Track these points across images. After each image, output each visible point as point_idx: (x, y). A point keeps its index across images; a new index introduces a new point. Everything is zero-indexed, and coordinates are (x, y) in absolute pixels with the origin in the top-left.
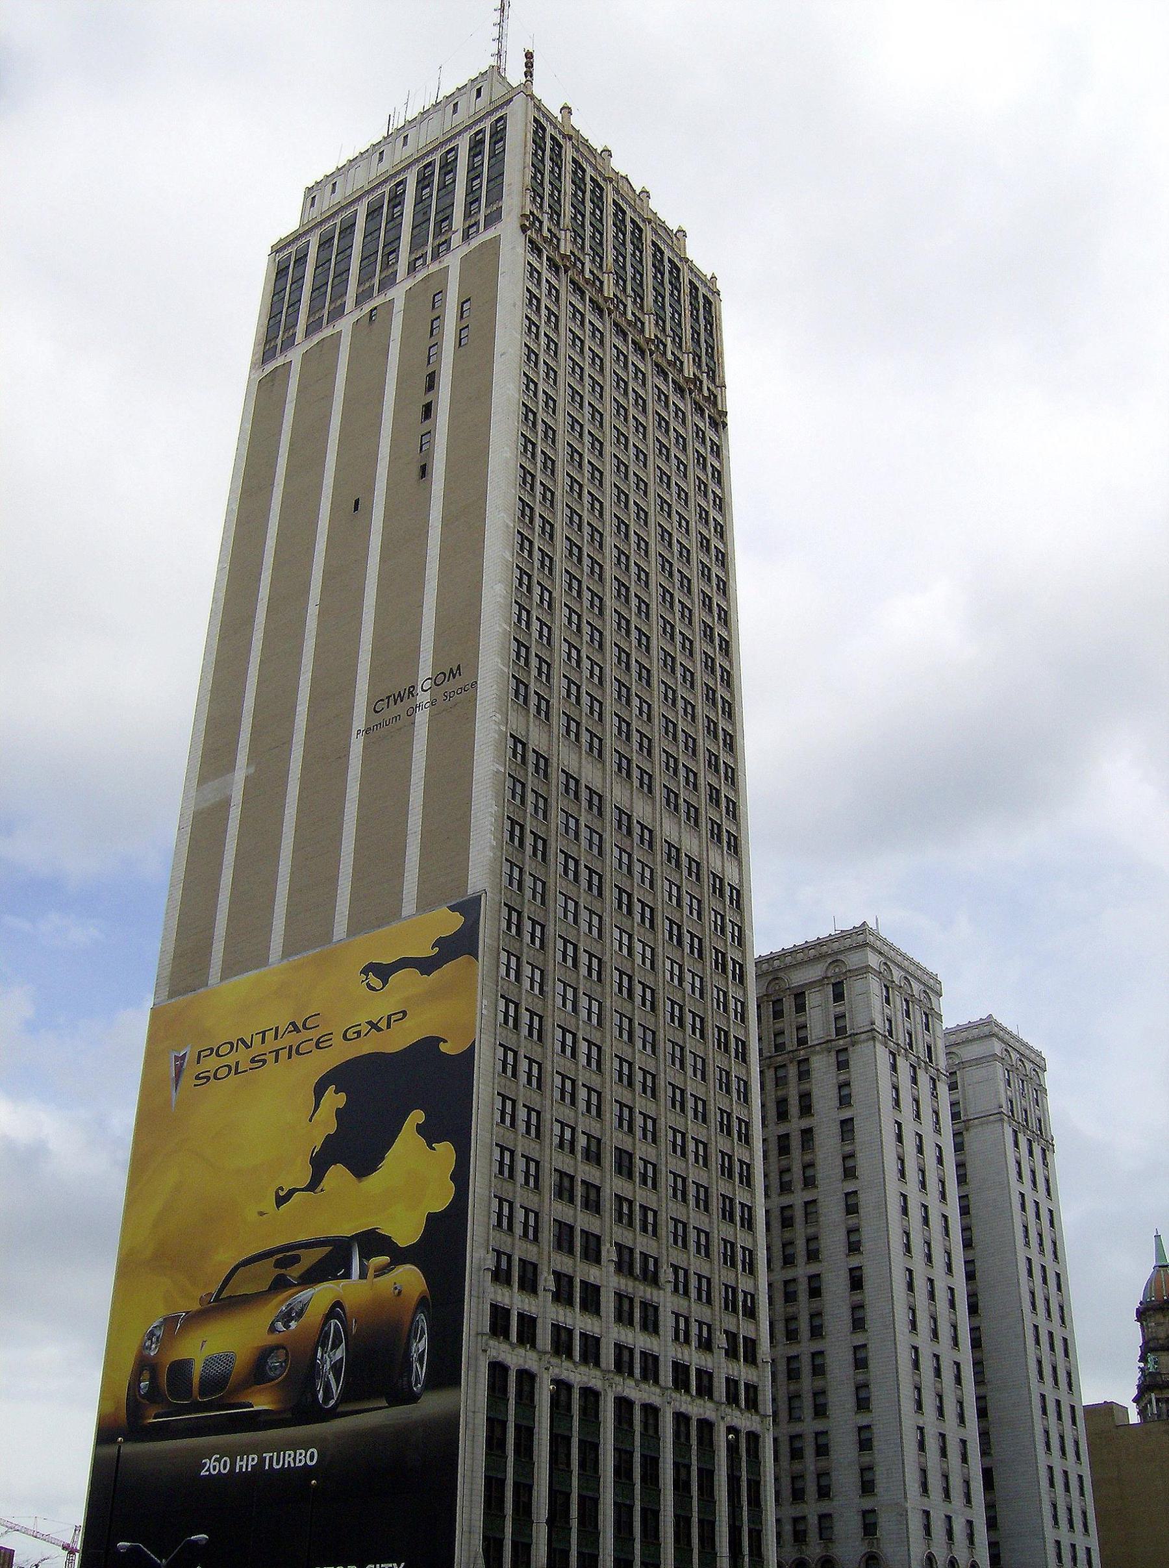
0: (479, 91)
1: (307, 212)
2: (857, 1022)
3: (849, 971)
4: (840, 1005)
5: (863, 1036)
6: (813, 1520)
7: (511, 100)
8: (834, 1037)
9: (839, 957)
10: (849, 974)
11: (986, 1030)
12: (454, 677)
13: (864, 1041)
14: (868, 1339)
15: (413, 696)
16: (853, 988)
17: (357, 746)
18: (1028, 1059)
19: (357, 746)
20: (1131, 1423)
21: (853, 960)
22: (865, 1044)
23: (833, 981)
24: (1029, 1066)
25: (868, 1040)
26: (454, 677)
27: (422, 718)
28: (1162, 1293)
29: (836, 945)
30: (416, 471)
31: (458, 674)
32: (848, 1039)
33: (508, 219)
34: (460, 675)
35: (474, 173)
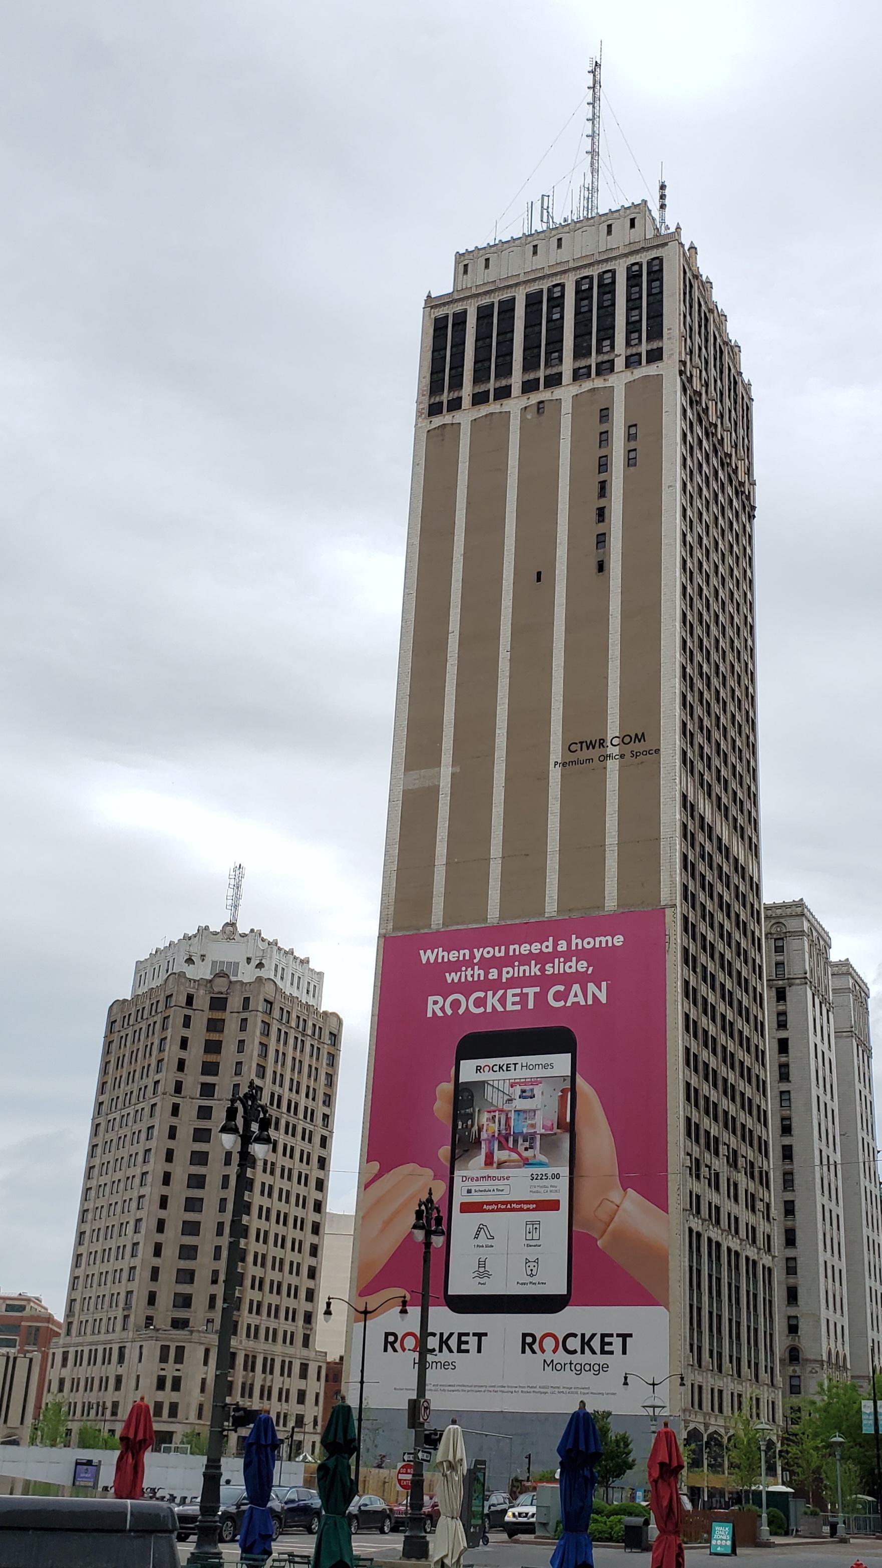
0: (632, 222)
1: (460, 279)
2: (793, 970)
3: (789, 932)
4: (780, 955)
5: (798, 981)
6: (109, 1405)
7: (666, 244)
8: (774, 977)
9: (782, 920)
10: (788, 934)
11: (844, 969)
12: (639, 741)
13: (798, 985)
14: (795, 1197)
15: (604, 747)
16: (791, 944)
17: (555, 775)
18: (864, 992)
19: (555, 775)
20: (430, 1308)
21: (792, 925)
22: (800, 987)
23: (775, 936)
24: (863, 994)
25: (801, 984)
26: (639, 741)
27: (613, 766)
28: (814, 1163)
29: (779, 912)
30: (594, 567)
31: (642, 740)
32: (786, 981)
33: (669, 362)
34: (644, 741)
35: (633, 304)
